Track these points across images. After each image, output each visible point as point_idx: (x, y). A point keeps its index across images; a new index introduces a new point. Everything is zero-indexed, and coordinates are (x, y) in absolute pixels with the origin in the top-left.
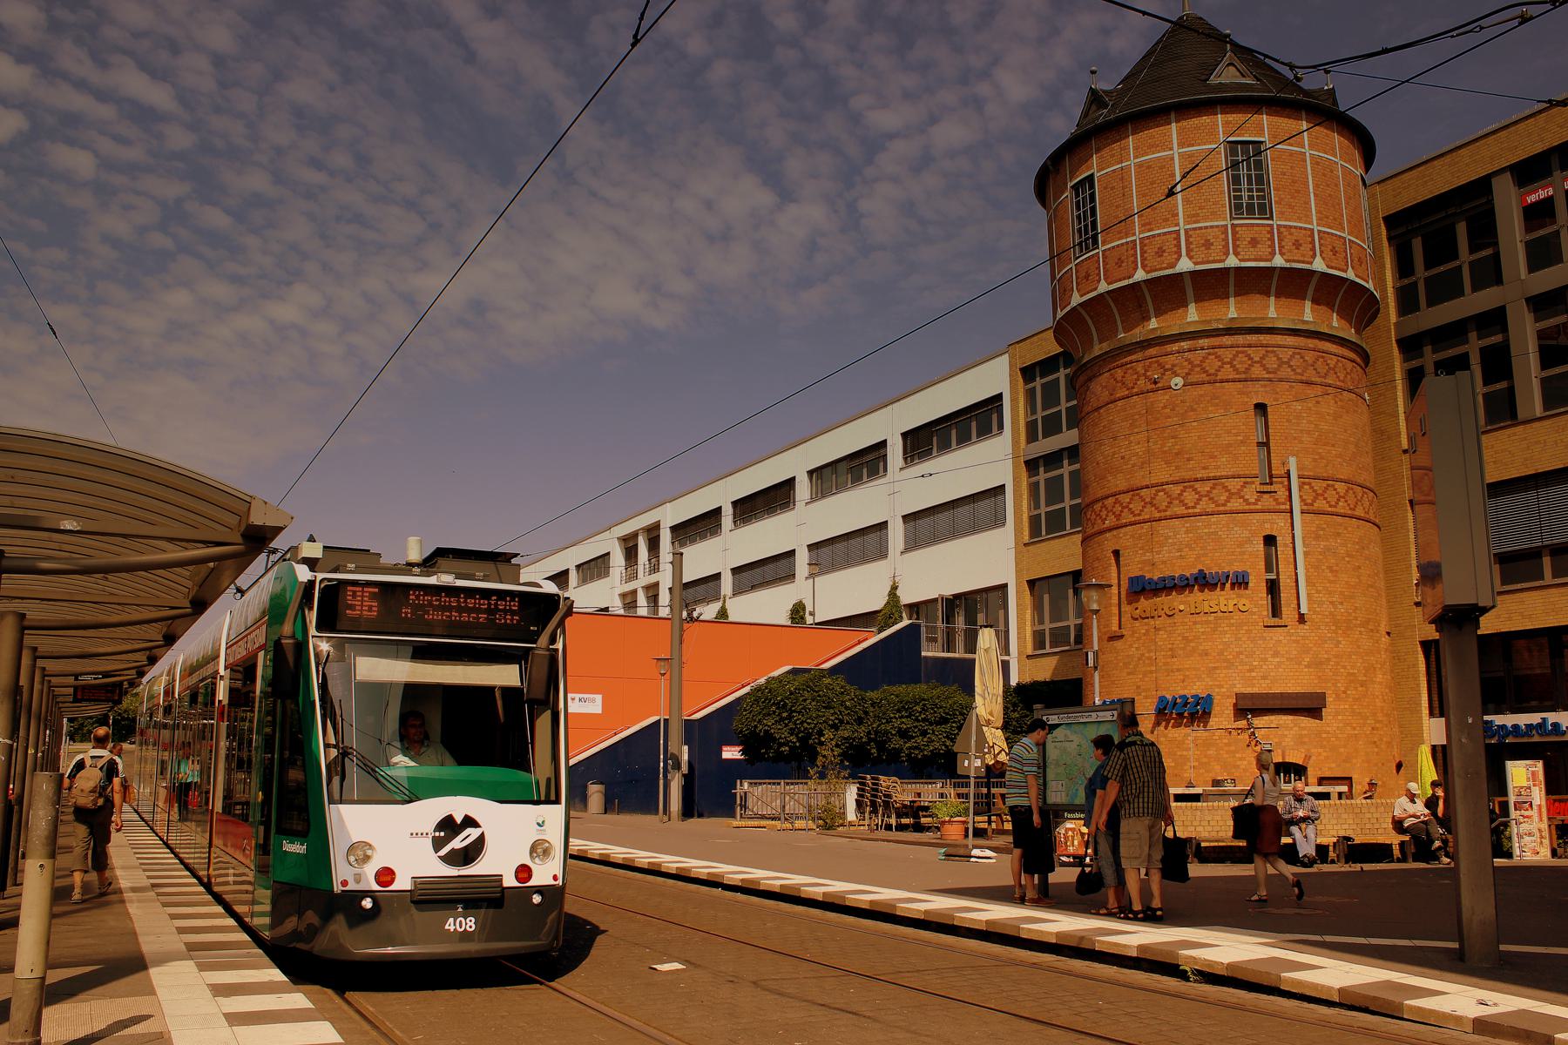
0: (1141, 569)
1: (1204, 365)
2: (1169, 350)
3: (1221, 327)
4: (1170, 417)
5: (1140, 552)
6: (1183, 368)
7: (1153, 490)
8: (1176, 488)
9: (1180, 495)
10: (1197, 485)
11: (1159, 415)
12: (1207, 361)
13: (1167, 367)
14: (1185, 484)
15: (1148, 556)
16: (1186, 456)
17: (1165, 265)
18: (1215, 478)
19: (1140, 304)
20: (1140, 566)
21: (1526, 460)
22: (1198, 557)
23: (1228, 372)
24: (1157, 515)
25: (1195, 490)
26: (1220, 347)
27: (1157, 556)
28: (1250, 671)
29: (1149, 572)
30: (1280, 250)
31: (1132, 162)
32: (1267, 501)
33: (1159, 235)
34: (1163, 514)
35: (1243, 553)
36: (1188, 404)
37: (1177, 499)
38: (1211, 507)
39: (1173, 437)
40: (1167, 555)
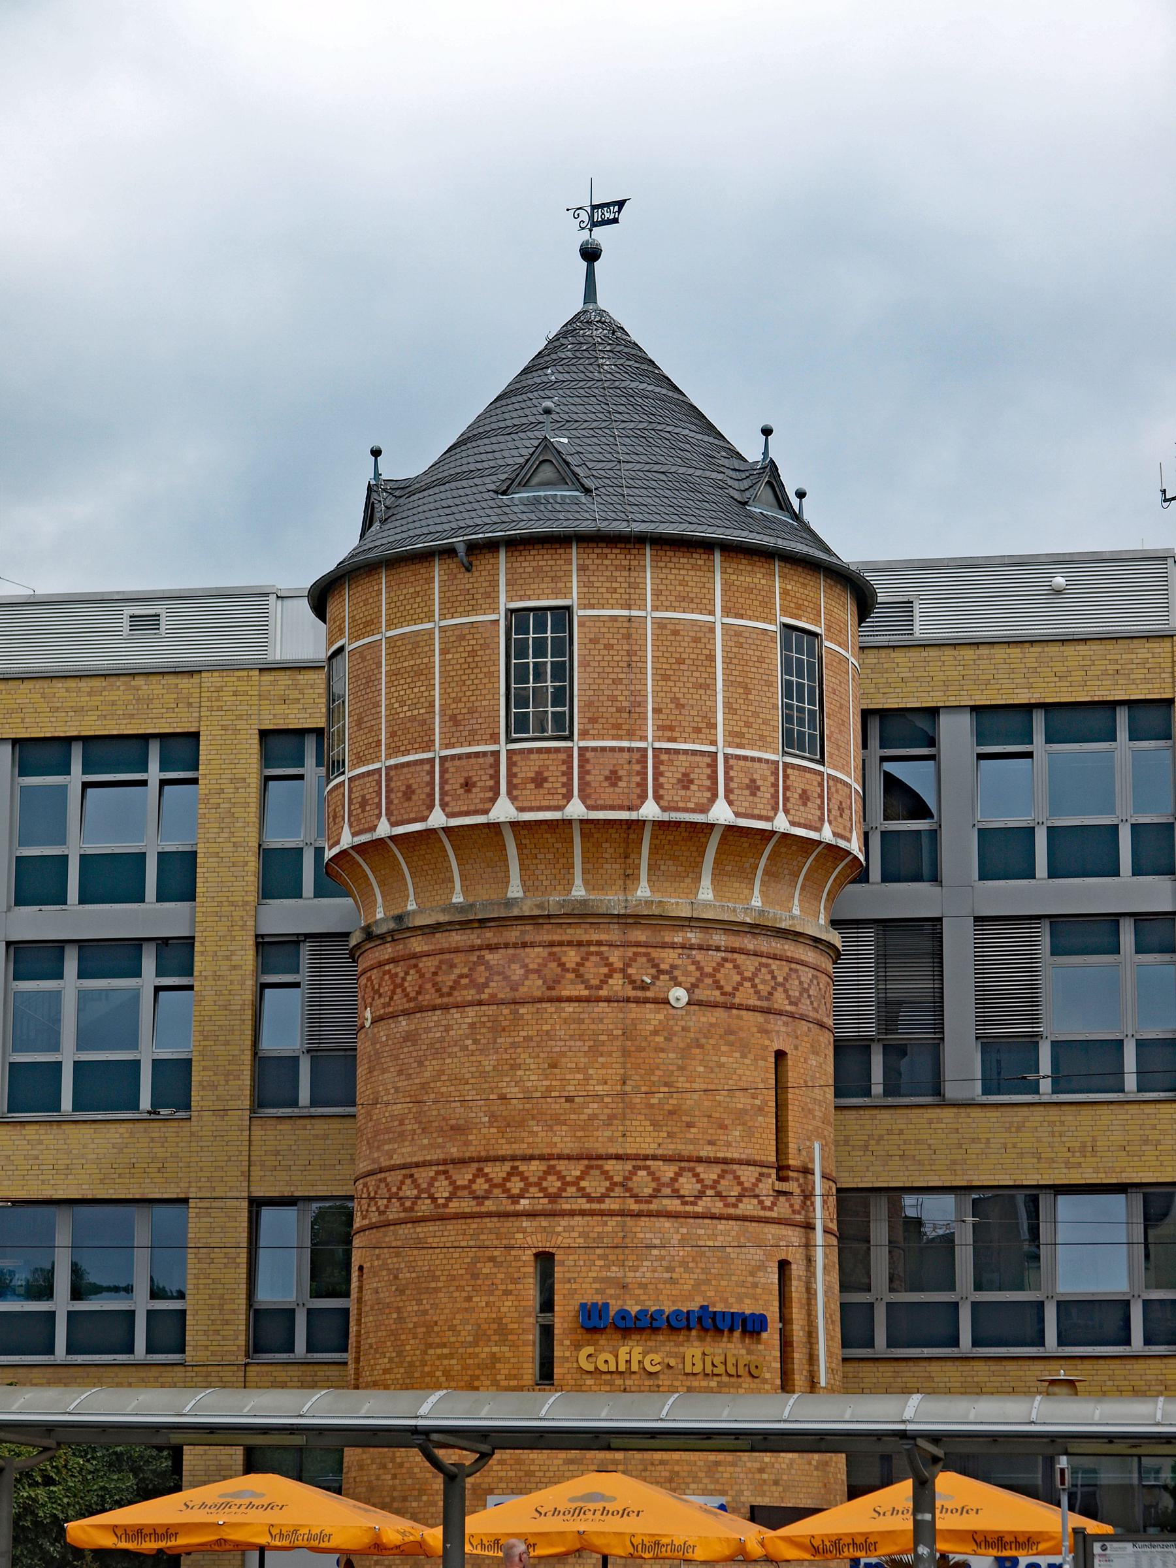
0: (598, 1291)
1: (718, 975)
2: (667, 939)
3: (748, 920)
4: (662, 1050)
5: (598, 1263)
6: (687, 973)
7: (629, 1166)
8: (666, 1168)
9: (674, 1180)
10: (700, 1169)
11: (644, 1044)
12: (722, 970)
13: (662, 966)
14: (683, 1164)
15: (615, 1272)
16: (684, 1118)
17: (691, 805)
18: (725, 1161)
19: (628, 854)
20: (597, 1286)
21: (954, 1162)
22: (698, 1284)
23: (746, 995)
24: (635, 1207)
25: (696, 1175)
26: (741, 951)
27: (632, 1274)
28: (761, 1470)
29: (617, 1298)
30: (655, 792)
31: (648, 614)
32: (782, 1209)
33: (686, 752)
34: (644, 1207)
35: (755, 1285)
36: (692, 1035)
37: (668, 1185)
38: (718, 1207)
39: (666, 1084)
40: (648, 1275)
